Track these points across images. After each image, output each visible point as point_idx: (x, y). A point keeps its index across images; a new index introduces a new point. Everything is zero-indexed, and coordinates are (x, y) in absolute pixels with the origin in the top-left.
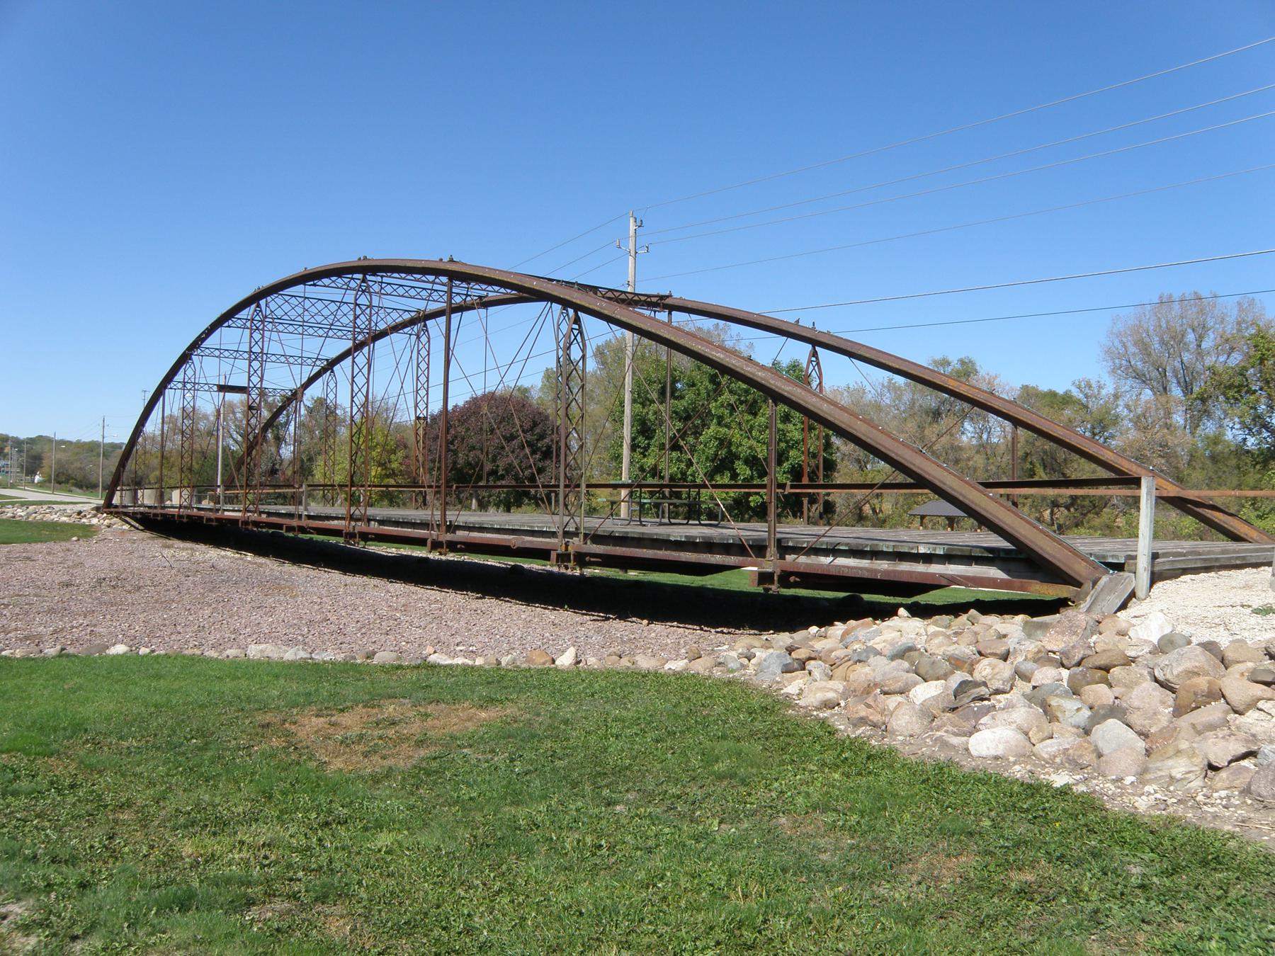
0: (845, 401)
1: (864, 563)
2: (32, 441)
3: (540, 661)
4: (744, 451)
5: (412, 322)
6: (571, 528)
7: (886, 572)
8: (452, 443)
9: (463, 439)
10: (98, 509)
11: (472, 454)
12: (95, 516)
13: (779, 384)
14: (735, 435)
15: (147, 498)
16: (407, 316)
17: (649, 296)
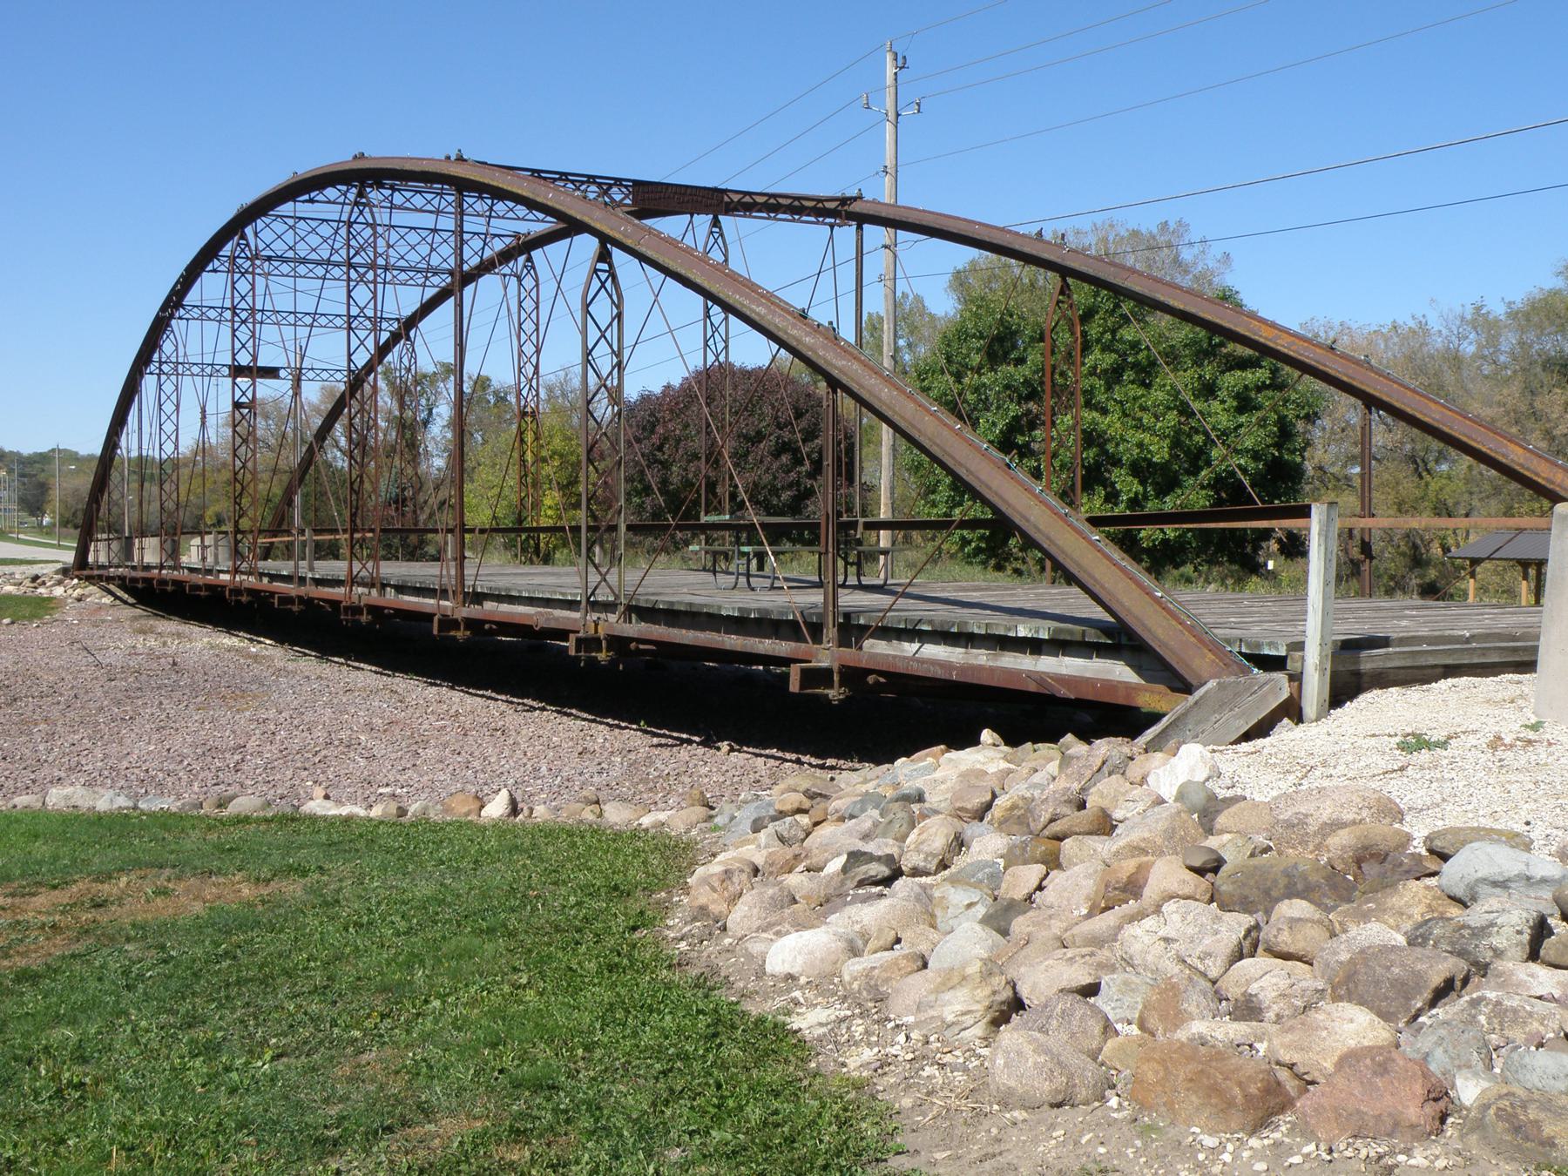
0: (1384, 355)
1: (980, 657)
2: (43, 459)
3: (461, 808)
4: (1128, 452)
5: (506, 256)
6: (603, 595)
7: (964, 669)
8: (660, 448)
9: (678, 441)
10: (65, 572)
11: (692, 467)
12: (60, 583)
13: (830, 356)
14: (1111, 424)
15: (149, 552)
16: (498, 245)
17: (819, 200)
